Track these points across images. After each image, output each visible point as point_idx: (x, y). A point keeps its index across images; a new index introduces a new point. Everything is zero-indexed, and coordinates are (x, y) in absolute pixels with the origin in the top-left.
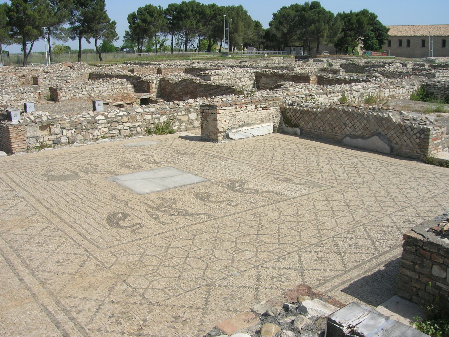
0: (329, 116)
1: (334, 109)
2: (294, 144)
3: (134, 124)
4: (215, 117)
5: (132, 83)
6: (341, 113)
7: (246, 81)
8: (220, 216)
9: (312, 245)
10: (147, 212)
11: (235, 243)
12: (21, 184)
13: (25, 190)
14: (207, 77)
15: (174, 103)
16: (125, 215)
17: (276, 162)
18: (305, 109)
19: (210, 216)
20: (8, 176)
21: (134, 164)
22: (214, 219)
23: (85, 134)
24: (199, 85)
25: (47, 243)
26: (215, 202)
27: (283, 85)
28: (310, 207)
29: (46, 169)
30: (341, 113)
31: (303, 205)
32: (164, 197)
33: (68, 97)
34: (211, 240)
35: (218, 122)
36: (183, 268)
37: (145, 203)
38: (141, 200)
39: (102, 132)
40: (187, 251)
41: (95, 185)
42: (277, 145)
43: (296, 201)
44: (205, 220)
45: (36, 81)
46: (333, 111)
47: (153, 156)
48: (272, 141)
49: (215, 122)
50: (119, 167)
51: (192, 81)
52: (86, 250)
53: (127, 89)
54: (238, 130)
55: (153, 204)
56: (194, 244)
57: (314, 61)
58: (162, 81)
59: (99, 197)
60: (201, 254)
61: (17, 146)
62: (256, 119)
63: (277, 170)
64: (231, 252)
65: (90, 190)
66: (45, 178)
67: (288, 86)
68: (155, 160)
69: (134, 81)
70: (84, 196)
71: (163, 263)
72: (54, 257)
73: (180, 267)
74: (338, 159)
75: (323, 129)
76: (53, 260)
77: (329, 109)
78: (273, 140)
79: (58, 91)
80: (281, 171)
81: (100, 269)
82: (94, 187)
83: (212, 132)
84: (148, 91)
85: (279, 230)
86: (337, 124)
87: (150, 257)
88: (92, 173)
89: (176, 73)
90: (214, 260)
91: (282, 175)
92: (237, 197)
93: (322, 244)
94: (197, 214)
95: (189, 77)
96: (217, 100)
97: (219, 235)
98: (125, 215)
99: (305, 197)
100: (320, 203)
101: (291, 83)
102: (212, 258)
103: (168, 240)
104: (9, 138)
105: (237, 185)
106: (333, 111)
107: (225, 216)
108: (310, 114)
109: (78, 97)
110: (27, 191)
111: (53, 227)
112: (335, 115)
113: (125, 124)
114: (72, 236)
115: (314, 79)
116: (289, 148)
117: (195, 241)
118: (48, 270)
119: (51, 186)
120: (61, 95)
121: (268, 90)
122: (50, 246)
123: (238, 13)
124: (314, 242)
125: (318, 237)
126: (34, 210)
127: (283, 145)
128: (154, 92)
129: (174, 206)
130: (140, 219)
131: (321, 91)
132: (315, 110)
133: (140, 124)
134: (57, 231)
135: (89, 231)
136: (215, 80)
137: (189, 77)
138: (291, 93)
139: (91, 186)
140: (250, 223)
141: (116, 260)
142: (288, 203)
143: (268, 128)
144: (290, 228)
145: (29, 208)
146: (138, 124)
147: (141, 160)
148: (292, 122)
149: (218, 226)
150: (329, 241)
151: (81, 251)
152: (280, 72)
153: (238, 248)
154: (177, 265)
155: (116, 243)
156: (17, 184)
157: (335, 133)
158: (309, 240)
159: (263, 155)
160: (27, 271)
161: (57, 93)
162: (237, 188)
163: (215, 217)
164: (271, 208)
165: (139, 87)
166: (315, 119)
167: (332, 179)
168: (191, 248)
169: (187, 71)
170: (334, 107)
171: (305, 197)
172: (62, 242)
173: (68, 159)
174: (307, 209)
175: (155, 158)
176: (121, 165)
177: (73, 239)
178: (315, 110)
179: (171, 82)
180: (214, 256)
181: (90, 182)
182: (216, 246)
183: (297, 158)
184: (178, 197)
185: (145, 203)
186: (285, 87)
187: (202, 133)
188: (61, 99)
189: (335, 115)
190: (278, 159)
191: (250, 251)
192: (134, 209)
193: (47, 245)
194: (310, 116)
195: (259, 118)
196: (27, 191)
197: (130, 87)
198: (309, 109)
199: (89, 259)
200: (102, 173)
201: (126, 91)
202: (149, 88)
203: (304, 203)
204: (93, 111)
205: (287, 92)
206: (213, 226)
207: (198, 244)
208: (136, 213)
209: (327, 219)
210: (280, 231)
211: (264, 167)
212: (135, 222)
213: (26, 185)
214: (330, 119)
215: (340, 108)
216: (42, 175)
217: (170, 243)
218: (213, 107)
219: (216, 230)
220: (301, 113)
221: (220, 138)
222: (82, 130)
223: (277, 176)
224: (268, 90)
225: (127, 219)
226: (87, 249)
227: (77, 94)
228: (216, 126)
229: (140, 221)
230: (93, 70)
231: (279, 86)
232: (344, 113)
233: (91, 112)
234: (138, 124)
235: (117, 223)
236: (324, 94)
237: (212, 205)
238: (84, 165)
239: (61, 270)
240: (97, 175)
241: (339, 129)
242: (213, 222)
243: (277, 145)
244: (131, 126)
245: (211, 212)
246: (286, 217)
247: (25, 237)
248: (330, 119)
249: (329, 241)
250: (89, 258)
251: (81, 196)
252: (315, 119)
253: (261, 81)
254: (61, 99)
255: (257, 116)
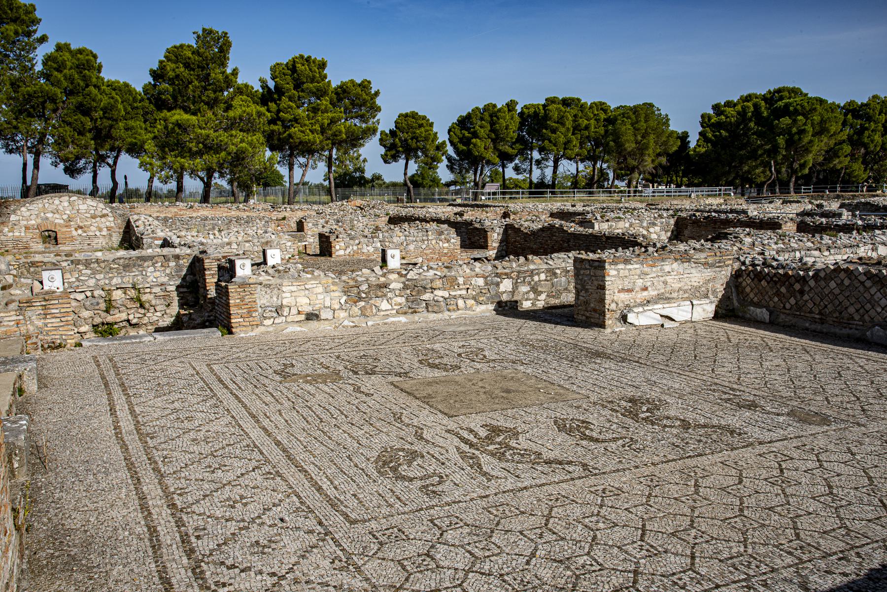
0: (833, 284)
1: (847, 270)
2: (759, 339)
3: (453, 293)
4: (601, 283)
5: (458, 234)
6: (863, 278)
7: (659, 233)
8: (608, 469)
9: (830, 555)
10: (458, 448)
11: (640, 532)
12: (232, 386)
13: (237, 397)
14: (586, 223)
15: (527, 259)
16: (413, 455)
17: (722, 369)
18: (781, 271)
19: (585, 466)
20: (212, 370)
21: (445, 360)
22: (596, 475)
23: (364, 307)
24: (573, 235)
25: (244, 501)
26: (597, 440)
27: (731, 234)
28: (810, 464)
29: (285, 362)
30: (863, 278)
31: (792, 459)
32: (494, 423)
33: (348, 250)
34: (587, 520)
35: (607, 292)
36: (522, 581)
37: (457, 435)
38: (449, 428)
39: (395, 305)
40: (532, 540)
41: (367, 395)
42: (722, 339)
43: (774, 449)
44: (575, 475)
45: (300, 226)
46: (842, 275)
47: (483, 350)
48: (711, 332)
49: (601, 291)
50: (417, 365)
51: (561, 229)
52: (320, 523)
53: (448, 241)
54: (646, 308)
55: (471, 437)
56: (550, 526)
57: (785, 202)
58: (508, 228)
59: (370, 418)
60: (564, 550)
61: (241, 320)
62: (680, 289)
63: (727, 384)
64: (634, 552)
65: (356, 402)
66: (278, 378)
67: (742, 236)
68: (485, 356)
69: (463, 230)
70: (342, 413)
71: (478, 566)
72: (252, 534)
73: (515, 579)
74: (859, 369)
75: (820, 311)
76: (246, 539)
77: (834, 270)
78: (714, 331)
79: (332, 240)
80: (735, 386)
81: (341, 569)
82: (364, 398)
83: (595, 310)
84: (485, 246)
85: (741, 510)
86: (853, 300)
87: (452, 548)
88: (367, 373)
89: (533, 214)
90: (593, 568)
91: (738, 393)
92: (643, 432)
93: (858, 555)
94: (561, 463)
95: (557, 222)
96: (606, 255)
97: (603, 512)
98: (413, 455)
99: (796, 443)
100: (833, 457)
101: (748, 230)
102: (589, 563)
103: (495, 512)
104: (228, 305)
105: (644, 408)
106: (842, 275)
107: (618, 470)
108: (792, 280)
109: (365, 251)
110: (240, 401)
111: (268, 468)
112: (847, 282)
113: (436, 292)
114: (299, 490)
115: (789, 228)
116: (747, 344)
117: (551, 521)
118: (229, 562)
119: (285, 391)
120: (338, 247)
121: (702, 241)
122: (251, 507)
123: (643, 115)
124: (834, 549)
125: (843, 536)
126: (242, 433)
127: (734, 340)
128: (494, 249)
129: (513, 443)
130: (443, 464)
131: (810, 244)
132: (801, 273)
133: (464, 292)
134: (273, 479)
135: (336, 483)
136: (601, 227)
137: (557, 222)
138: (750, 247)
139: (358, 395)
140: (674, 491)
141: (379, 550)
142: (757, 451)
143: (706, 309)
144: (769, 509)
145: (233, 430)
146: (459, 292)
147: (460, 355)
148: (752, 300)
149: (604, 491)
150: (874, 549)
151: (311, 523)
152: (723, 216)
153: (648, 544)
154: (508, 574)
155: (385, 510)
156: (224, 384)
157: (848, 320)
158: (821, 540)
159: (695, 356)
160: (185, 560)
161: (331, 243)
162: (643, 415)
163: (597, 471)
164: (719, 460)
165: (470, 239)
166: (802, 292)
167: (852, 408)
168: (541, 536)
169: (552, 215)
170: (845, 266)
171: (796, 443)
172: (277, 501)
173: (327, 347)
174: (804, 468)
175: (486, 353)
176: (421, 362)
177: (299, 497)
178: (801, 273)
179: (525, 231)
180: (592, 557)
181: (358, 390)
182: (599, 536)
183: (767, 363)
184: (523, 425)
185: (457, 435)
186: (735, 237)
187: (577, 298)
188: (337, 253)
189: (847, 282)
190: (726, 365)
191: (676, 554)
192: (433, 443)
193: (245, 505)
194: (791, 285)
195: (686, 287)
196: (240, 401)
197: (456, 240)
198: (790, 272)
199: (321, 543)
200: (384, 374)
201: (446, 245)
202: (486, 241)
203: (795, 455)
204: (381, 267)
205: (738, 245)
206: (591, 489)
207: (558, 527)
208: (435, 451)
209: (858, 494)
210: (746, 513)
211: (699, 377)
212: (431, 470)
213: (240, 388)
214: (837, 291)
215: (860, 269)
216: (275, 372)
217: (497, 519)
218: (600, 265)
219: (600, 499)
220: (772, 278)
221: (608, 322)
222: (360, 299)
223: (726, 396)
224: (702, 241)
225: (415, 463)
226: (323, 520)
227: (365, 246)
228: (602, 300)
229: (440, 470)
230: (393, 209)
231: (725, 236)
232: (868, 279)
233: (377, 269)
234: (459, 292)
235: (394, 470)
236: (816, 250)
237: (592, 445)
238: (353, 359)
239: (257, 562)
240: (373, 377)
241: (857, 311)
242: (592, 480)
243: (722, 339)
244: (447, 296)
245: (587, 460)
246: (757, 482)
247: (206, 486)
248: (837, 291)
249: (874, 549)
250: (323, 540)
251: (336, 413)
252: (802, 292)
253: (685, 229)
254: (337, 253)
255: (682, 284)
